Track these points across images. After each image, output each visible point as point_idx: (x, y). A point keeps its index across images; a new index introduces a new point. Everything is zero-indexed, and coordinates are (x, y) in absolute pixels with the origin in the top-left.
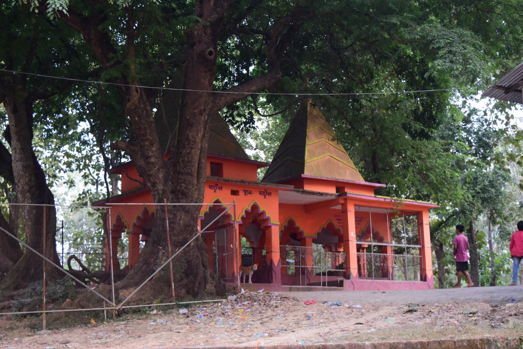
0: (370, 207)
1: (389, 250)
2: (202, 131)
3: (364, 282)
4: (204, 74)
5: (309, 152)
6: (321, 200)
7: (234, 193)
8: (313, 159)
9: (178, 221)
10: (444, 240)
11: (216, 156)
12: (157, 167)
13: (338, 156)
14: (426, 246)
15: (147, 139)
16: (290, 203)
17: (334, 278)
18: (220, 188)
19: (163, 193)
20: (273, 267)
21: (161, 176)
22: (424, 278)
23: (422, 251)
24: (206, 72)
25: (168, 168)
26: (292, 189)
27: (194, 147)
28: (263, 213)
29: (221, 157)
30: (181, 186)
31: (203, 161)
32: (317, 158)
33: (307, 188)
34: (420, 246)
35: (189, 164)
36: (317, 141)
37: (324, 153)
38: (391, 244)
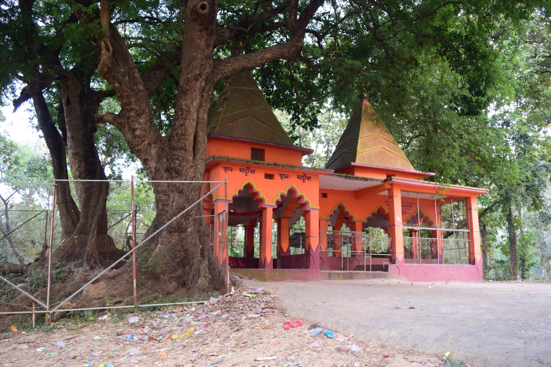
0: (417, 193)
2: (198, 99)
4: (199, 33)
5: (361, 143)
7: (269, 176)
9: (171, 203)
11: (255, 142)
12: (146, 142)
14: (474, 230)
15: (132, 109)
17: (378, 262)
18: (253, 172)
20: (311, 252)
21: (153, 152)
22: (472, 261)
23: (470, 235)
24: (201, 31)
25: (163, 144)
26: (333, 173)
27: (188, 117)
29: (262, 142)
34: (469, 231)
35: (182, 137)
36: (370, 134)
37: (376, 145)
38: (441, 228)
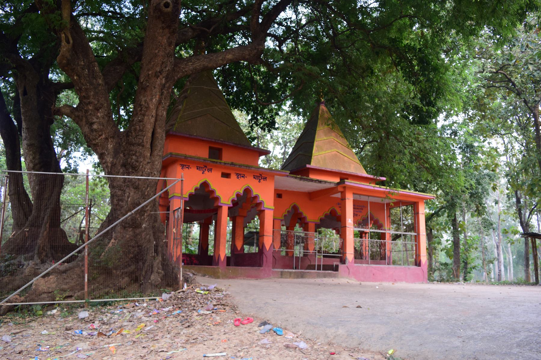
0: (369, 196)
1: (387, 236)
2: (157, 96)
3: (359, 266)
4: (161, 31)
5: (316, 146)
6: (323, 188)
7: (226, 175)
8: (321, 153)
9: (126, 199)
10: (433, 226)
11: (213, 140)
12: (104, 136)
13: (344, 152)
14: (421, 234)
15: (90, 103)
16: (295, 190)
17: (329, 262)
18: (210, 170)
19: (112, 166)
20: (264, 251)
21: (110, 146)
22: (418, 263)
23: (417, 238)
24: (163, 28)
26: (288, 174)
27: (147, 113)
28: (256, 197)
30: (132, 159)
31: (159, 130)
32: (324, 153)
33: (312, 176)
34: (416, 234)
35: (140, 133)
37: (331, 149)
